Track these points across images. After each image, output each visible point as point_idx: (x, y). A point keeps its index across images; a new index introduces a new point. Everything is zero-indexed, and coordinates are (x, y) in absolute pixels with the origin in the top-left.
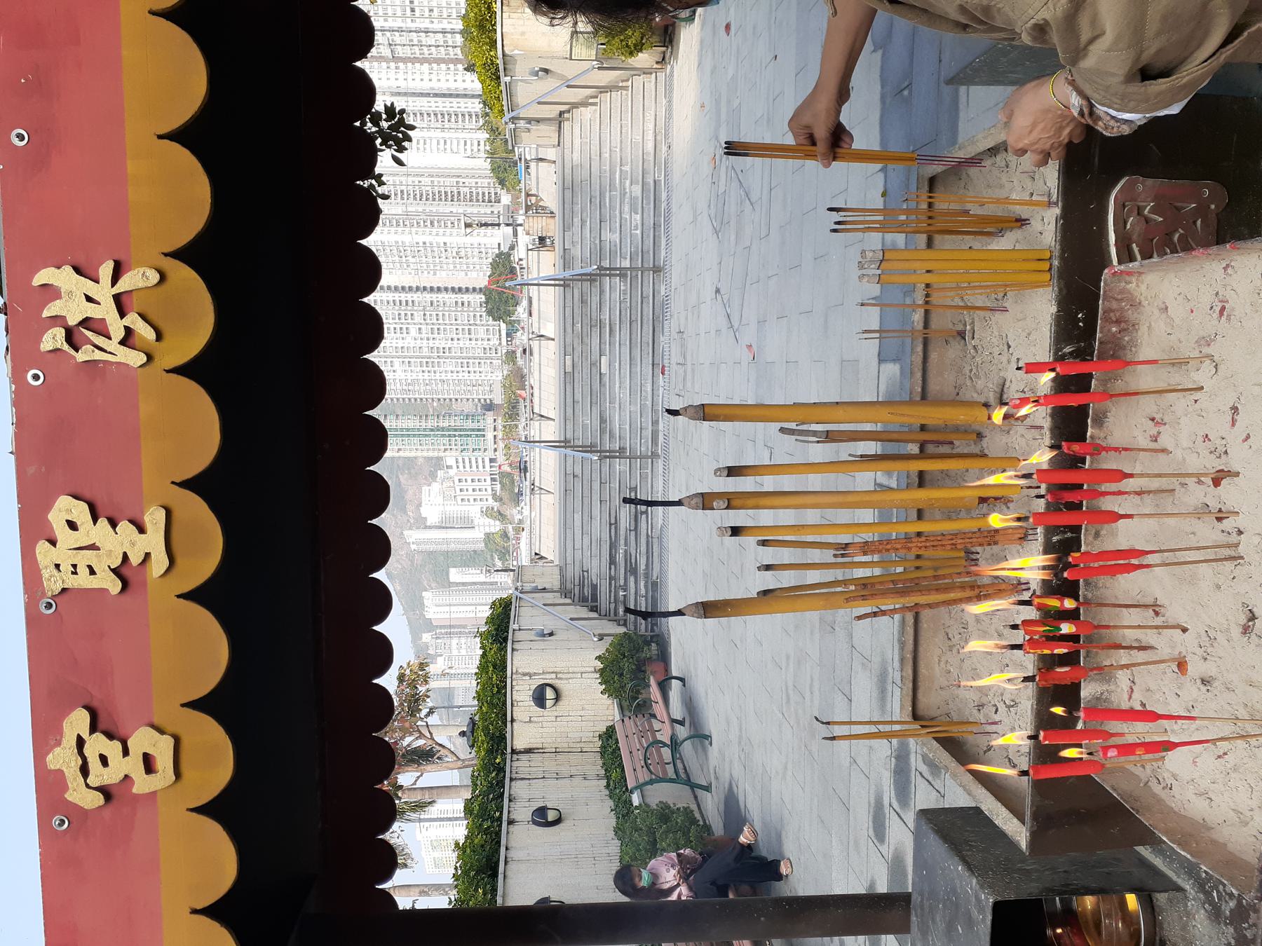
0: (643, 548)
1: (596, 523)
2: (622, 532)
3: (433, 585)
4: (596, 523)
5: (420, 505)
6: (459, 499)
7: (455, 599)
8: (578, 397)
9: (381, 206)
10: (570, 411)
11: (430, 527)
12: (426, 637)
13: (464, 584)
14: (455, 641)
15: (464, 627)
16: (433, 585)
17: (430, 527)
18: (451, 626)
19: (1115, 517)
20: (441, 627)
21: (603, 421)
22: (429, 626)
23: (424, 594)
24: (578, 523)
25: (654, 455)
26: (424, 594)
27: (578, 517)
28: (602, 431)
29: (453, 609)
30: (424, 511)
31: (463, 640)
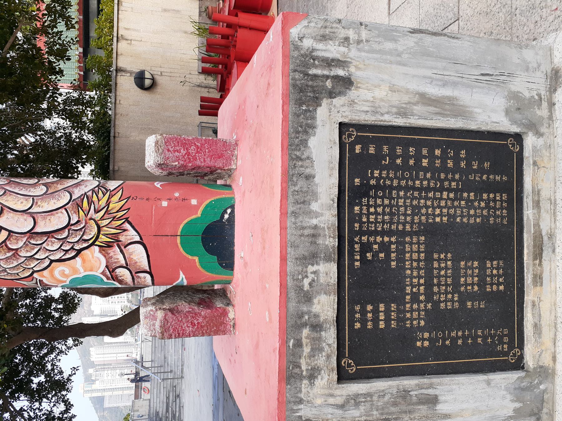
0: (178, 409)
1: (162, 395)
2: (171, 401)
3: (96, 344)
4: (162, 395)
5: (90, 304)
6: (110, 302)
7: (107, 350)
8: (157, 345)
9: (77, 322)
10: (154, 349)
11: (95, 316)
12: (91, 371)
13: (111, 343)
14: (106, 372)
15: (111, 365)
16: (96, 344)
17: (95, 316)
18: (104, 365)
19: (359, 87)
20: (99, 365)
21: (165, 358)
22: (92, 365)
23: (91, 349)
24: (155, 392)
25: (182, 377)
26: (91, 349)
27: (155, 390)
28: (165, 362)
29: (105, 356)
30: (93, 308)
31: (109, 372)
